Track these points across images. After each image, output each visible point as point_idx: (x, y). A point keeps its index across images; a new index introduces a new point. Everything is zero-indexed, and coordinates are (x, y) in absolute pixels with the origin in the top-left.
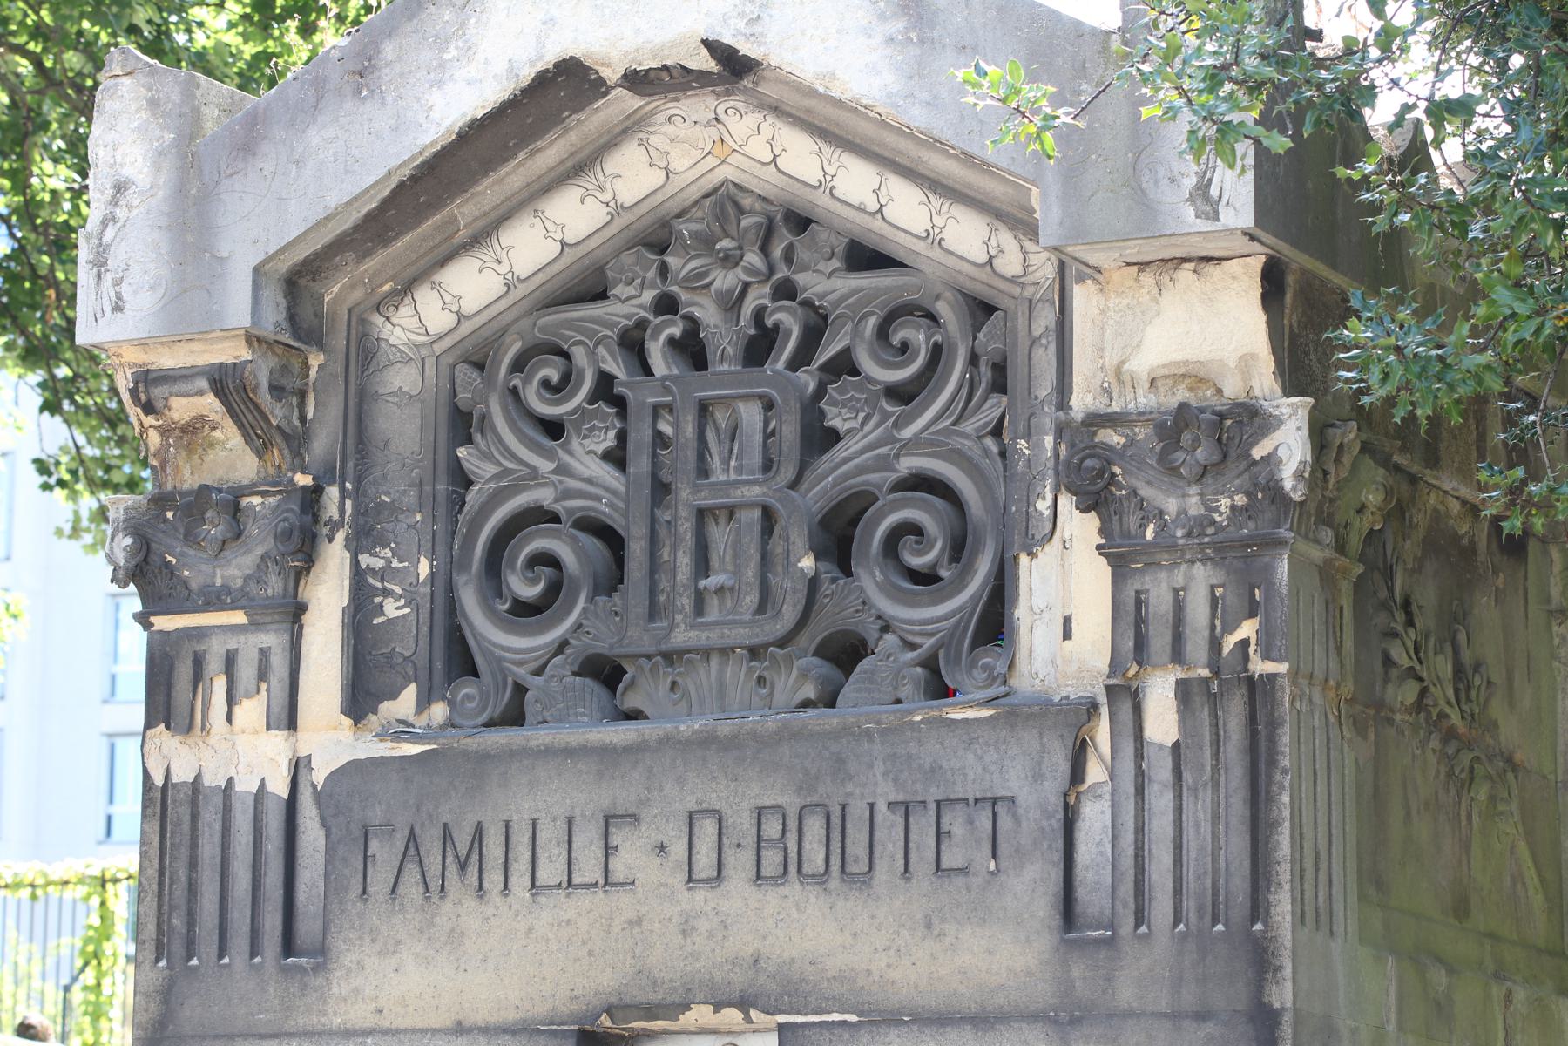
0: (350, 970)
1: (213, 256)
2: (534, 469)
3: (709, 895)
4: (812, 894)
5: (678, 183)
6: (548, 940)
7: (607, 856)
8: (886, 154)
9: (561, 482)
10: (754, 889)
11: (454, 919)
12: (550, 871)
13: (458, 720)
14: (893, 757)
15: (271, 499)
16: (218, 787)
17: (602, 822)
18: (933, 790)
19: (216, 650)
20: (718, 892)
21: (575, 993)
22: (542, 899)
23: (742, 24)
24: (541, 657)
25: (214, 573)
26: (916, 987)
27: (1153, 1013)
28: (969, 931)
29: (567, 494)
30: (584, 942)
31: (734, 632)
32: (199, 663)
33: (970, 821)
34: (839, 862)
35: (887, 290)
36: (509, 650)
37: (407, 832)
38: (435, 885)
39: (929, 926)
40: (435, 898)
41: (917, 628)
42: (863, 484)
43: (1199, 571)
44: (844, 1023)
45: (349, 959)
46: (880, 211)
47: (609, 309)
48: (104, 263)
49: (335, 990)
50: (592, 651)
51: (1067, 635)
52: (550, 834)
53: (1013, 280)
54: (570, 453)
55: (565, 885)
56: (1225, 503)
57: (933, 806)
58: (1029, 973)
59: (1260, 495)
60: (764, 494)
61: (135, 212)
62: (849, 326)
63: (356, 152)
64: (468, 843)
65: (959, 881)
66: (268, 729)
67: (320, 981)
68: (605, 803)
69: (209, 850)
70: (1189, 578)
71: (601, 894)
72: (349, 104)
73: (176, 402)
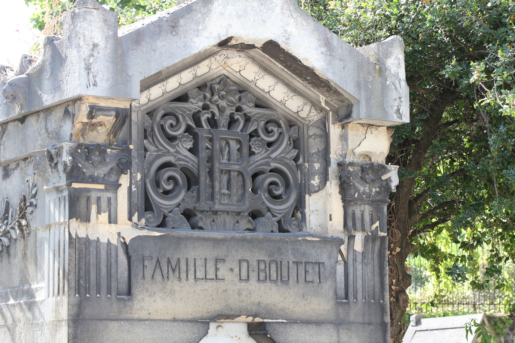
0: (140, 300)
1: (127, 74)
2: (169, 150)
3: (246, 284)
4: (273, 285)
5: (212, 72)
6: (200, 295)
7: (216, 271)
8: (282, 78)
9: (177, 155)
10: (257, 283)
11: (172, 287)
12: (200, 274)
13: (148, 224)
14: (294, 249)
15: (114, 151)
16: (95, 240)
17: (215, 261)
18: (304, 259)
19: (94, 196)
20: (248, 283)
21: (208, 311)
22: (198, 282)
23: (285, 40)
24: (172, 207)
25: (95, 171)
26: (301, 313)
27: (358, 323)
28: (314, 298)
29: (179, 159)
30: (210, 296)
31: (232, 207)
32: (88, 199)
33: (313, 269)
34: (280, 277)
35: (267, 114)
36: (161, 204)
37: (156, 259)
38: (165, 276)
39: (303, 296)
40: (166, 280)
41: (277, 211)
42: (262, 169)
43: (367, 206)
44: (283, 322)
45: (139, 297)
46: (269, 92)
47: (190, 106)
48: (90, 69)
49: (135, 307)
50: (187, 208)
51: (331, 220)
53: (303, 118)
54: (179, 147)
55: (204, 279)
56: (374, 190)
57: (304, 263)
58: (329, 311)
59: (383, 189)
60: (239, 168)
61: (100, 55)
62: (256, 123)
63: (172, 51)
64: (175, 264)
65: (311, 284)
66: (110, 222)
67: (130, 303)
68: (216, 255)
69: (93, 260)
70: (365, 208)
71: (215, 282)
72: (169, 36)
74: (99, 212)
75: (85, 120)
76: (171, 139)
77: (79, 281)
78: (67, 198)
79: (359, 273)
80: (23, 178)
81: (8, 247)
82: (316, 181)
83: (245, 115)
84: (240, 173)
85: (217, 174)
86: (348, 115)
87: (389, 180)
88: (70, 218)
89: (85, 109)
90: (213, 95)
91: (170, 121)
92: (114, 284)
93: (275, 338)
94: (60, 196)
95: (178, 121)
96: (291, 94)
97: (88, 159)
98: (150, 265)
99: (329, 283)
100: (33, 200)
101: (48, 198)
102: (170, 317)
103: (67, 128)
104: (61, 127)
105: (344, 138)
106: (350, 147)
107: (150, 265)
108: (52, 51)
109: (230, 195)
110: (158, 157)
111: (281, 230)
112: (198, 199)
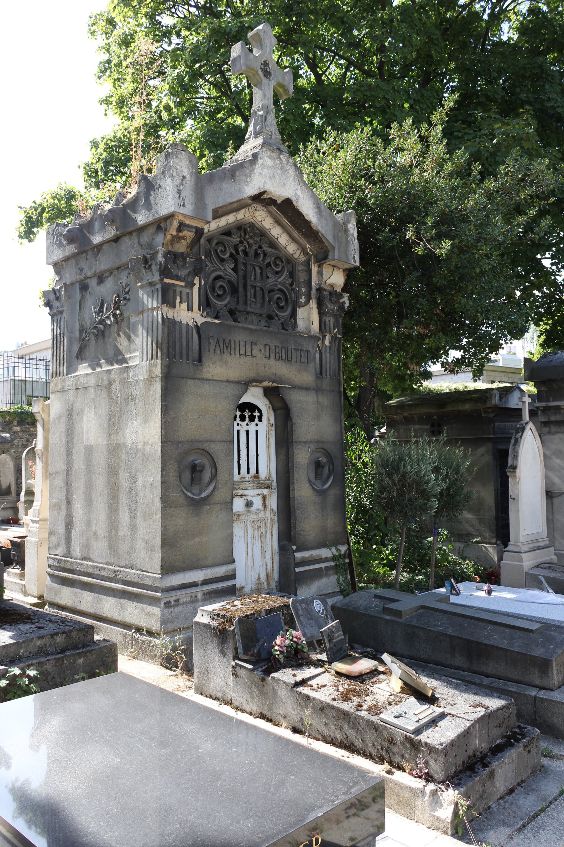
5: (246, 219)
12: (242, 352)
19: (178, 290)
29: (226, 275)
45: (207, 364)
52: (242, 344)
66: (188, 310)
69: (177, 335)
72: (230, 181)
73: (186, 232)
74: (181, 302)
75: (174, 233)
76: (222, 260)
77: (168, 349)
78: (160, 289)
79: (328, 359)
80: (117, 282)
81: (103, 332)
82: (303, 300)
83: (264, 251)
84: (262, 289)
85: (249, 288)
86: (325, 257)
87: (344, 303)
88: (163, 303)
89: (175, 224)
90: (245, 234)
91: (221, 248)
92: (191, 354)
93: (284, 397)
94: (153, 288)
95: (225, 249)
96: (291, 241)
97: (174, 263)
98: (213, 342)
99: (313, 364)
100: (126, 295)
101: (140, 292)
102: (225, 379)
103: (160, 239)
104: (153, 239)
105: (320, 273)
106: (324, 279)
107: (213, 342)
108: (146, 184)
109: (256, 303)
110: (213, 271)
111: (283, 329)
112: (238, 303)
